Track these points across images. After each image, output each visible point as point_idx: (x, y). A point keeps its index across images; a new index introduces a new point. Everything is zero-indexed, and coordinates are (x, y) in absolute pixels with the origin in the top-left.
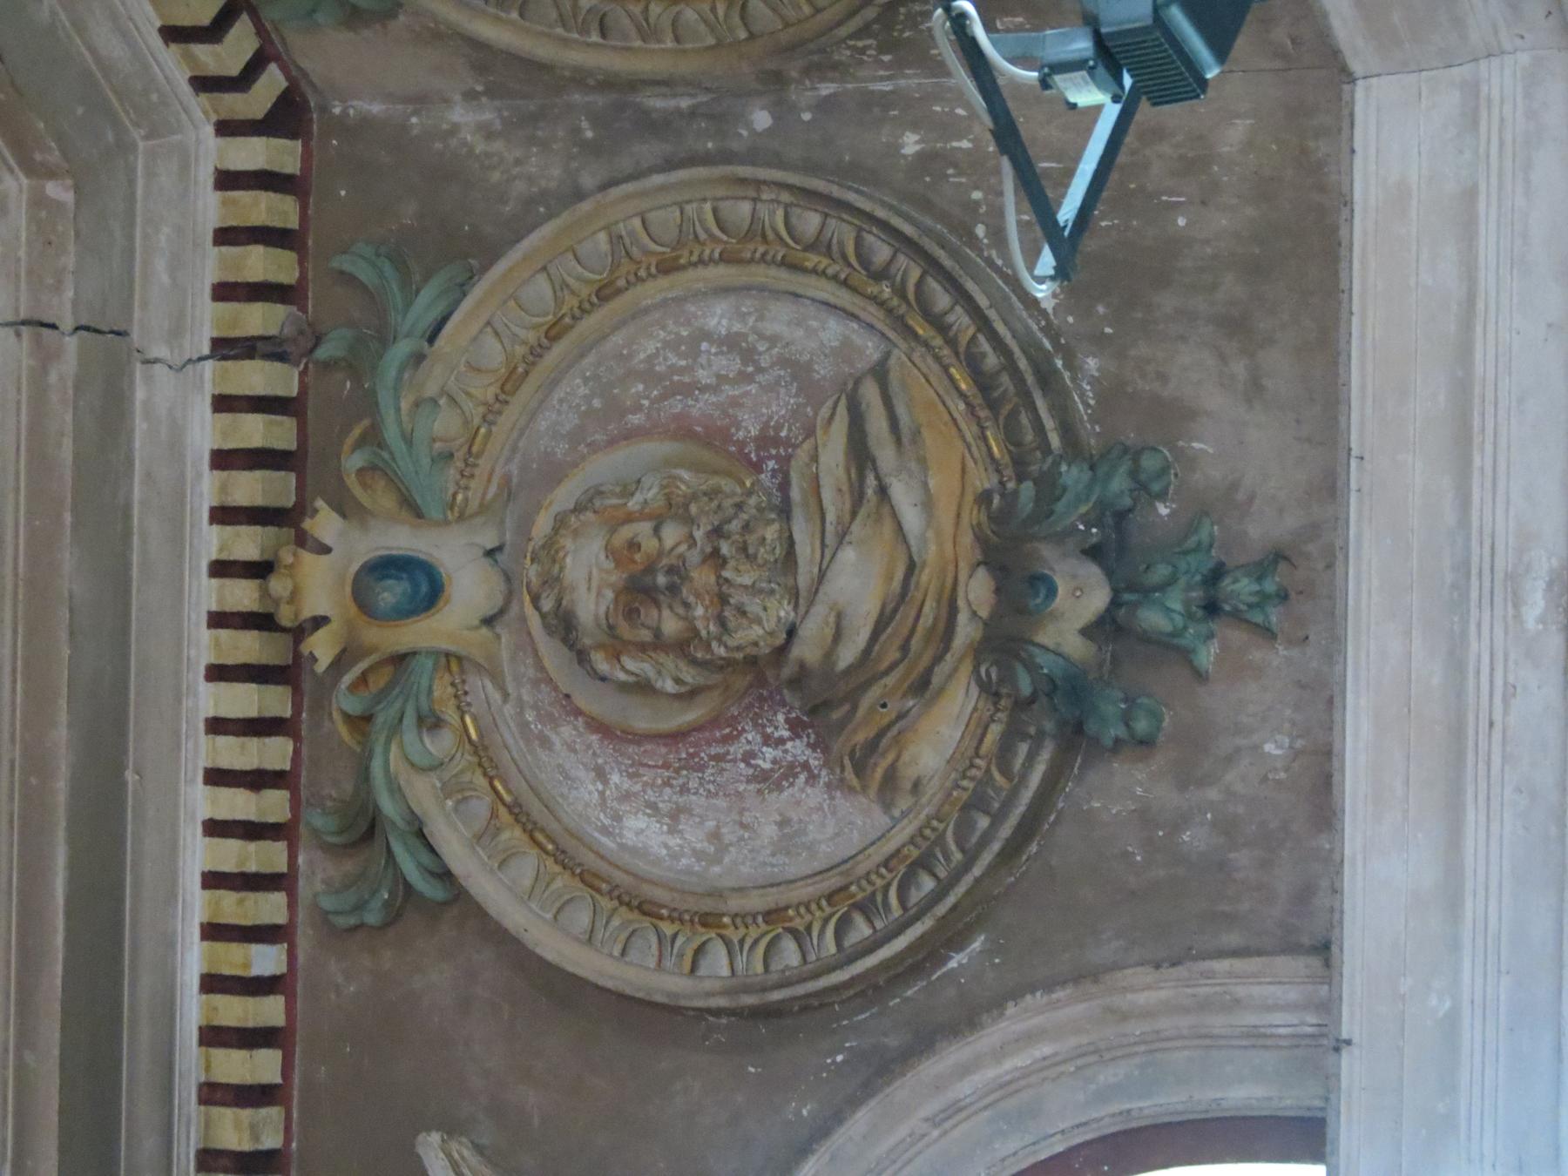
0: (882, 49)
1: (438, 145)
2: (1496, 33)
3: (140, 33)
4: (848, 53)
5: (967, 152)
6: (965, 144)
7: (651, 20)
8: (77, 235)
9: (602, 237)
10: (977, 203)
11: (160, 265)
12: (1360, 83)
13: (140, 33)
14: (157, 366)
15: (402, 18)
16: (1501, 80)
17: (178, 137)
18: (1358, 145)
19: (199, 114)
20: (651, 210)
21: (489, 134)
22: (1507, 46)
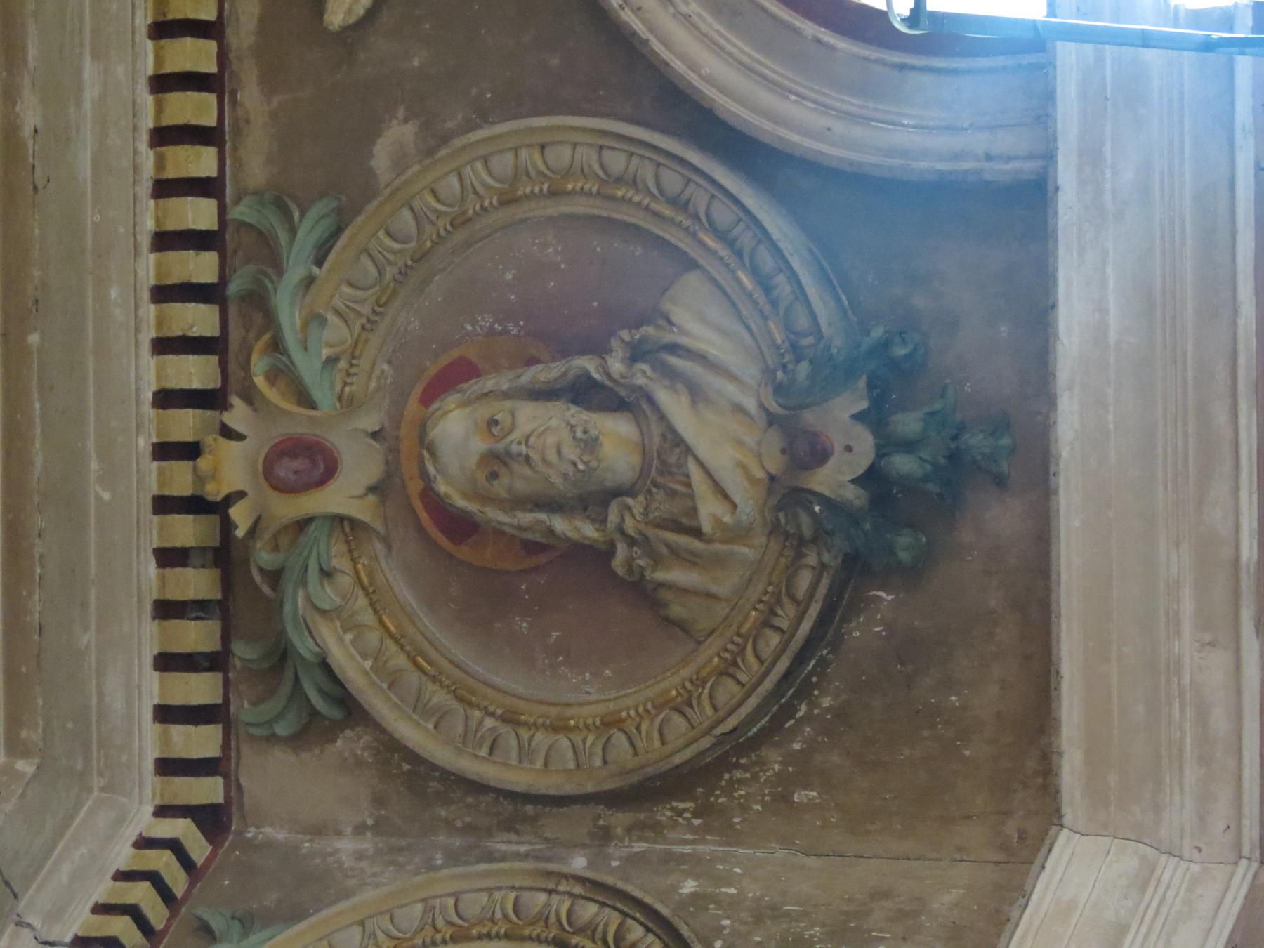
0: (696, 814)
1: (317, 861)
2: (1182, 837)
3: (139, 699)
4: (669, 813)
5: (732, 896)
6: (732, 891)
7: (533, 744)
8: (23, 795)
9: (419, 907)
10: (724, 928)
11: (66, 869)
12: (1065, 831)
13: (139, 699)
14: (26, 931)
15: (339, 743)
16: (1172, 872)
17: (125, 800)
18: (1049, 865)
19: (148, 792)
20: (466, 892)
21: (360, 856)
22: (1186, 855)
